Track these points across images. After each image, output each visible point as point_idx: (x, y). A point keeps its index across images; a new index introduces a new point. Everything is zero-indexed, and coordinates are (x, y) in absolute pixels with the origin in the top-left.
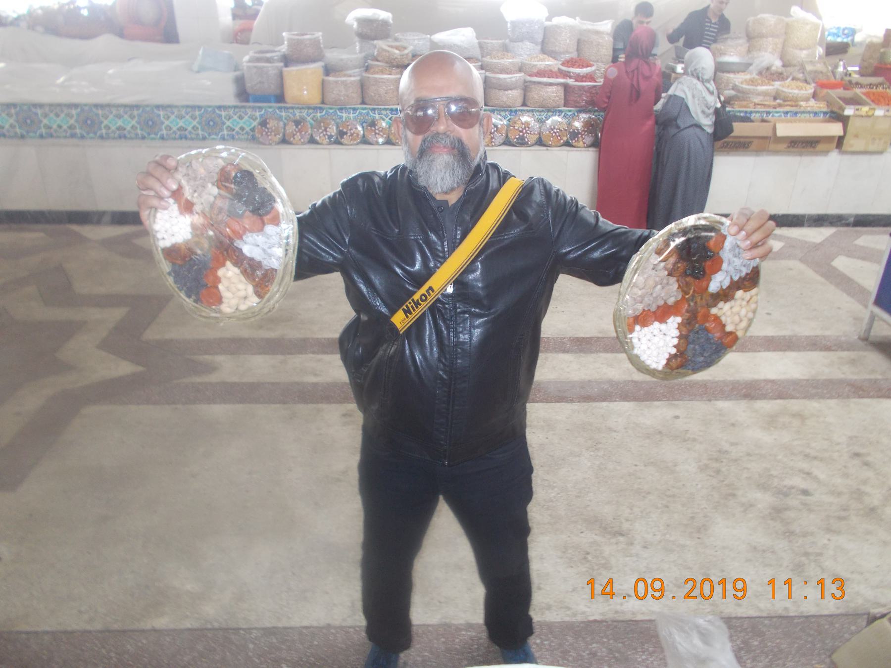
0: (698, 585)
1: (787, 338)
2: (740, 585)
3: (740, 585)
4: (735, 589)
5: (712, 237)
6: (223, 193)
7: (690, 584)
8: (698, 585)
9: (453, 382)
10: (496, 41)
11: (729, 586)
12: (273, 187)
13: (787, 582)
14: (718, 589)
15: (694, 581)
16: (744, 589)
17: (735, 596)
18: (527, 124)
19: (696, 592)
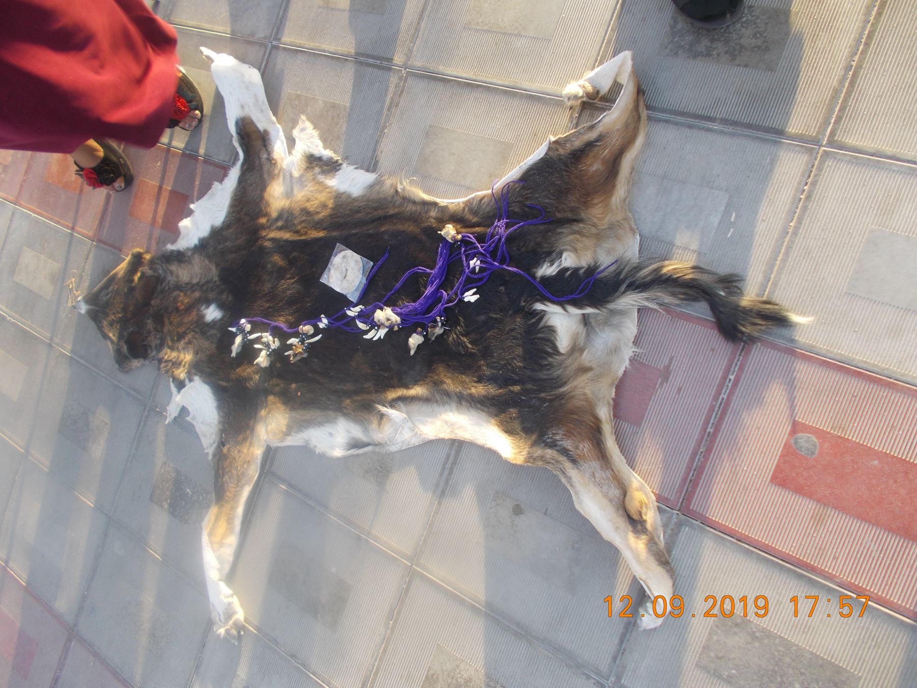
0: (719, 603)
1: (232, 210)
2: (761, 603)
3: (761, 603)
4: (757, 607)
5: (432, 273)
6: (138, 295)
7: (711, 601)
8: (719, 603)
9: (379, 134)
10: (781, 255)
11: (750, 602)
12: (236, 496)
13: (793, 599)
14: (739, 606)
15: (714, 598)
16: (766, 607)
17: (757, 614)
18: (197, 115)
19: (716, 611)
